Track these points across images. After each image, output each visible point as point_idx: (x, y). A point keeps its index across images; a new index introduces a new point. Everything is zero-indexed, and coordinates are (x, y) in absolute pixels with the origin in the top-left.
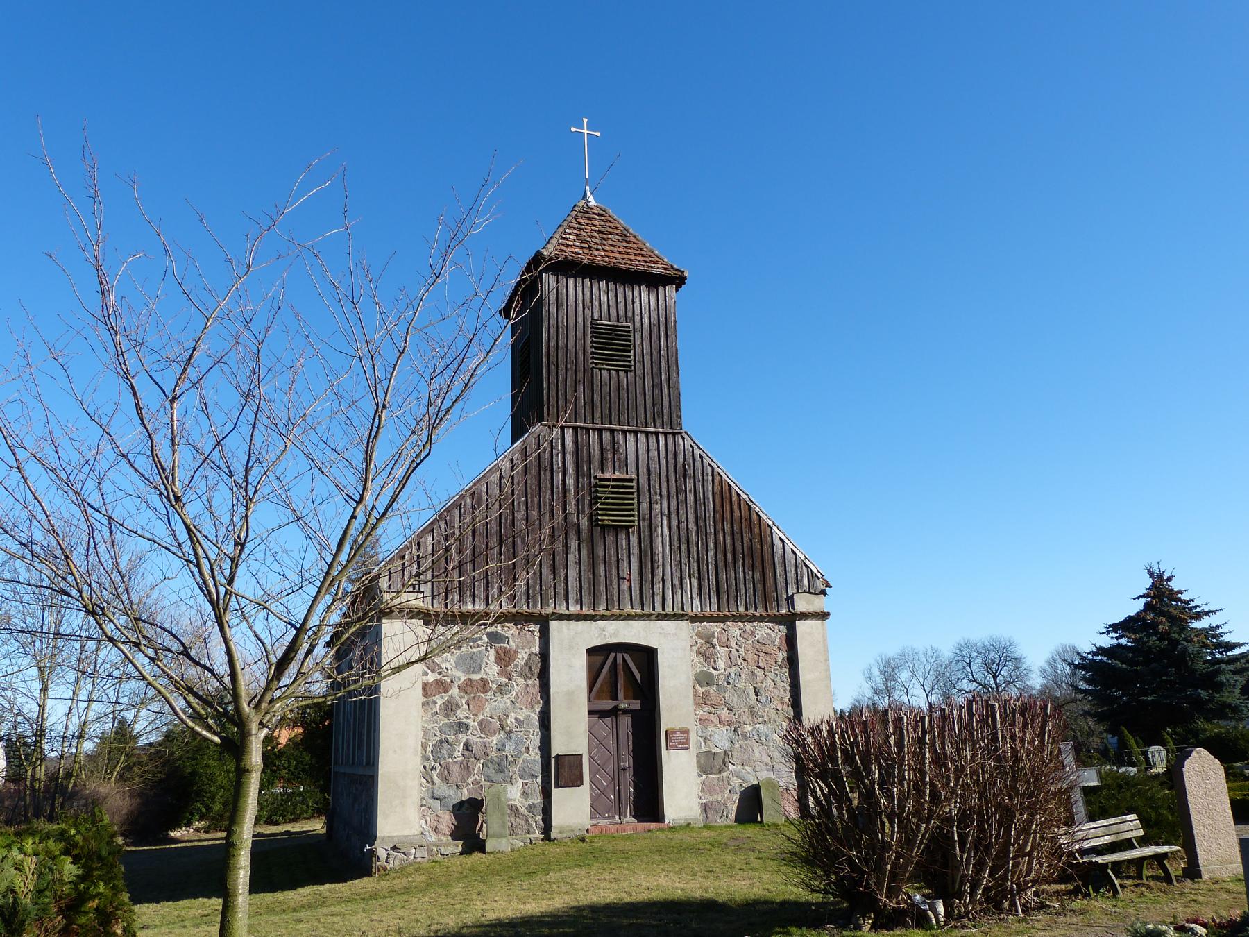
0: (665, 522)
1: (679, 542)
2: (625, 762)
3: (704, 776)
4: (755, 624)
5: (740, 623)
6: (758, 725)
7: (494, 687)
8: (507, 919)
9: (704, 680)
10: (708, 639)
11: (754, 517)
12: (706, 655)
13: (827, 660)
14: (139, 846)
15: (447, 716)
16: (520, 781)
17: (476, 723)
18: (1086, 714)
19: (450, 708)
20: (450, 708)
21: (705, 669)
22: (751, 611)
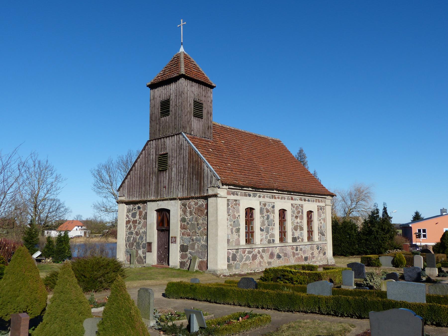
0: (175, 166)
1: (179, 172)
2: (166, 246)
3: (182, 253)
4: (198, 200)
5: (194, 200)
6: (197, 237)
7: (138, 222)
8: (394, 301)
9: (183, 220)
10: (184, 205)
11: (199, 159)
12: (184, 212)
13: (217, 213)
14: (422, 259)
15: (130, 230)
16: (142, 249)
17: (135, 232)
18: (46, 244)
19: (130, 228)
20: (130, 228)
21: (184, 216)
22: (196, 195)
